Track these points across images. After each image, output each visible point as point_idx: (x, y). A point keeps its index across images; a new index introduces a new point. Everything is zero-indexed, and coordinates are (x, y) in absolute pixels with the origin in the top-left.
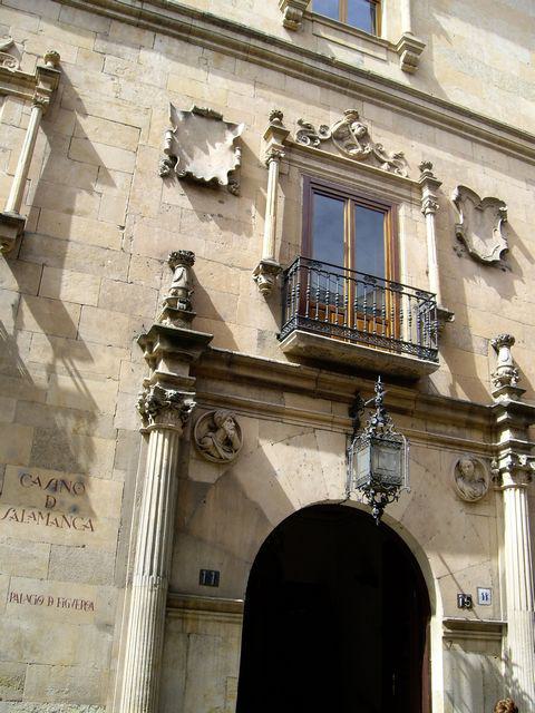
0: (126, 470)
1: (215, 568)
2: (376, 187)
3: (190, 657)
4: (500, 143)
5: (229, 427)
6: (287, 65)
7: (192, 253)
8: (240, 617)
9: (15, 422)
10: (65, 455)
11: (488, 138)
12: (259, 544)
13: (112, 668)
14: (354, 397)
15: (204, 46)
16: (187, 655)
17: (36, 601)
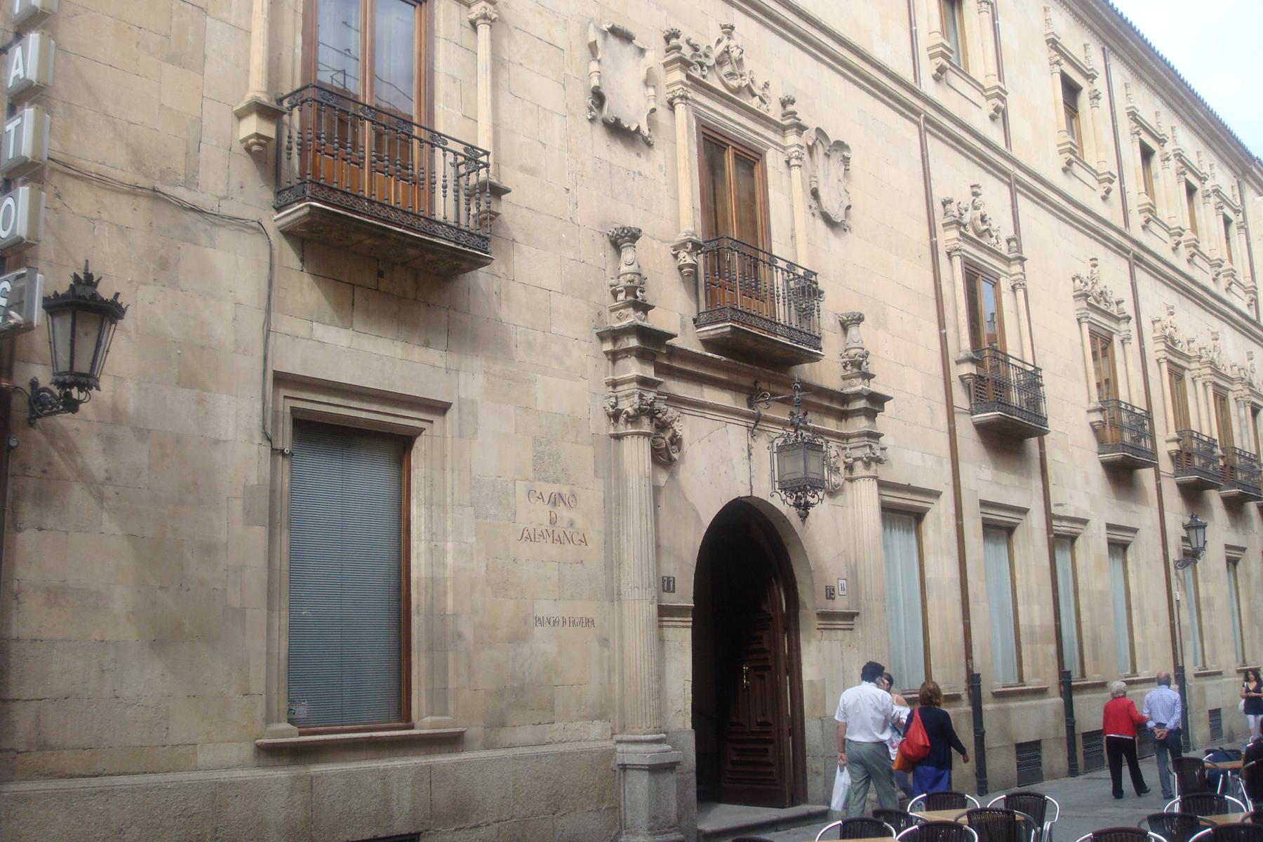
1: (672, 574)
7: (640, 231)
9: (516, 432)
12: (699, 544)
17: (554, 622)
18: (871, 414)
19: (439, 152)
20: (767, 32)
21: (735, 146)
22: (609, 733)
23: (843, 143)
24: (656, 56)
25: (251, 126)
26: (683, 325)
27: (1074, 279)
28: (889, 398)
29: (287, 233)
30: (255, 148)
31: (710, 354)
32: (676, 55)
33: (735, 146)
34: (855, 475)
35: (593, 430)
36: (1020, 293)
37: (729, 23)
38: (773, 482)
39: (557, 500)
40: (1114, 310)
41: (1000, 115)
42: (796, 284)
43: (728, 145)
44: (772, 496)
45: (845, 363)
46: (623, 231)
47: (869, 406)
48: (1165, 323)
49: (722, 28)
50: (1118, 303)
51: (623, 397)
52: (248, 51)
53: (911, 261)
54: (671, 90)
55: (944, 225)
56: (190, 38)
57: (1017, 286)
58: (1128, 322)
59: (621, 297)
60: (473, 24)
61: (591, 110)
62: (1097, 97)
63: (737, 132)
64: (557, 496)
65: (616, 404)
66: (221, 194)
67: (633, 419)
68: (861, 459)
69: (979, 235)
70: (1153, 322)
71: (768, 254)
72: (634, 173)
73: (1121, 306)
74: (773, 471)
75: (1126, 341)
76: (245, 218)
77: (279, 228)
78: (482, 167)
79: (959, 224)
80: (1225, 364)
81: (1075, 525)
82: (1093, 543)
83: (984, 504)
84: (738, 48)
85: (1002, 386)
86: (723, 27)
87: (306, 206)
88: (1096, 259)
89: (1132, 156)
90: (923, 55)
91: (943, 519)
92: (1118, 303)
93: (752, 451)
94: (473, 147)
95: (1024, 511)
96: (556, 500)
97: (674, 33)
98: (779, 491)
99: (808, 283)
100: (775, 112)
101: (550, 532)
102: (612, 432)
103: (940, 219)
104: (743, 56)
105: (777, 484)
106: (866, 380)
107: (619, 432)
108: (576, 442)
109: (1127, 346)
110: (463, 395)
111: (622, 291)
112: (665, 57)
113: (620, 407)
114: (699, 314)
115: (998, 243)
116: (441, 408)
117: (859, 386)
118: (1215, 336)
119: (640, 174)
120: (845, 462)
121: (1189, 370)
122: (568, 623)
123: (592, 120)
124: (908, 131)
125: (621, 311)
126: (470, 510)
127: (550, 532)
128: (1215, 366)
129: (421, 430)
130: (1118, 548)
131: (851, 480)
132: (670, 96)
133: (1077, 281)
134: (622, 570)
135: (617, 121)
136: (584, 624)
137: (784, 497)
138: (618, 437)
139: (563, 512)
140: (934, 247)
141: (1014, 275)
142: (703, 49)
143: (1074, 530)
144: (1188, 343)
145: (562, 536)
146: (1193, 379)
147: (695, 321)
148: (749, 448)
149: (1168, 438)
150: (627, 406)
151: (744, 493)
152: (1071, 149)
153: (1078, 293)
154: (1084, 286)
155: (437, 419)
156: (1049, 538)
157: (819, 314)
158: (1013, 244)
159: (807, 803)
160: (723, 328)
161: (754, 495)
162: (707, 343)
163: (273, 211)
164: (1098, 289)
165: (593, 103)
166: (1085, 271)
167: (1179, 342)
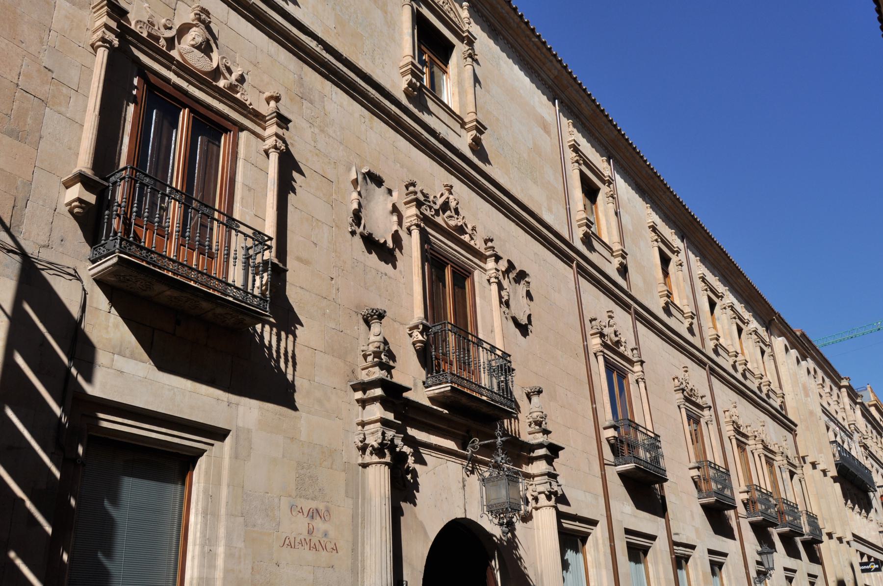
0: (353, 498)
7: (385, 312)
9: (284, 456)
14: (465, 434)
18: (549, 460)
19: (233, 232)
20: (474, 194)
21: (453, 265)
23: (525, 272)
24: (398, 196)
25: (76, 191)
26: (415, 385)
27: (674, 379)
28: (562, 448)
29: (99, 281)
30: (76, 210)
31: (435, 407)
32: (413, 197)
33: (453, 265)
34: (539, 505)
35: (345, 460)
36: (642, 385)
37: (450, 184)
38: (483, 505)
39: (315, 514)
40: (699, 401)
41: (623, 270)
42: (496, 363)
43: (448, 264)
44: (481, 517)
45: (530, 422)
46: (372, 312)
47: (549, 453)
48: (731, 413)
49: (445, 187)
50: (702, 397)
51: (370, 434)
52: (80, 139)
53: (571, 356)
54: (409, 220)
55: (592, 335)
56: (29, 121)
57: (640, 380)
58: (710, 410)
59: (370, 358)
60: (267, 152)
61: (352, 225)
62: (681, 265)
63: (455, 256)
64: (315, 511)
65: (365, 439)
66: (42, 243)
67: (379, 451)
68: (543, 493)
69: (612, 347)
70: (724, 412)
71: (475, 337)
72: (382, 273)
73: (704, 399)
74: (482, 497)
75: (709, 422)
76: (63, 264)
77: (92, 276)
78: (266, 249)
79: (602, 335)
80: (770, 442)
81: (687, 550)
82: (699, 562)
83: (628, 532)
84: (455, 200)
85: (633, 446)
86: (446, 186)
87: (115, 256)
88: (687, 367)
89: (705, 306)
90: (575, 225)
91: (600, 542)
92: (702, 397)
93: (465, 483)
94: (260, 233)
95: (653, 538)
96: (313, 514)
97: (412, 183)
98: (487, 513)
99: (505, 362)
100: (479, 245)
101: (308, 540)
102: (360, 461)
103: (589, 331)
104: (458, 206)
105: (485, 507)
106: (545, 435)
107: (365, 462)
108: (331, 468)
109: (710, 426)
110: (241, 424)
111: (370, 355)
112: (406, 198)
113: (367, 442)
114: (427, 378)
115: (626, 350)
116: (219, 434)
117: (540, 438)
118: (763, 424)
119: (386, 275)
120: (532, 495)
121: (749, 445)
123: (353, 233)
124: (568, 273)
125: (370, 369)
126: (241, 519)
127: (308, 540)
128: (765, 443)
129: (204, 451)
130: (716, 567)
131: (537, 509)
132: (409, 224)
133: (676, 380)
134: (365, 574)
135: (370, 235)
137: (491, 518)
138: (365, 466)
139: (318, 524)
140: (586, 349)
141: (637, 372)
142: (431, 198)
143: (687, 553)
144: (747, 427)
145: (317, 544)
146: (752, 451)
147: (424, 383)
148: (464, 480)
149: (741, 490)
150: (373, 441)
151: (460, 515)
152: (667, 294)
153: (678, 388)
154: (681, 384)
155: (217, 443)
156: (671, 558)
157: (512, 384)
158: (635, 352)
160: (446, 388)
161: (467, 517)
162: (431, 399)
163: (89, 263)
164: (690, 387)
165: (353, 220)
166: (681, 374)
167: (741, 426)
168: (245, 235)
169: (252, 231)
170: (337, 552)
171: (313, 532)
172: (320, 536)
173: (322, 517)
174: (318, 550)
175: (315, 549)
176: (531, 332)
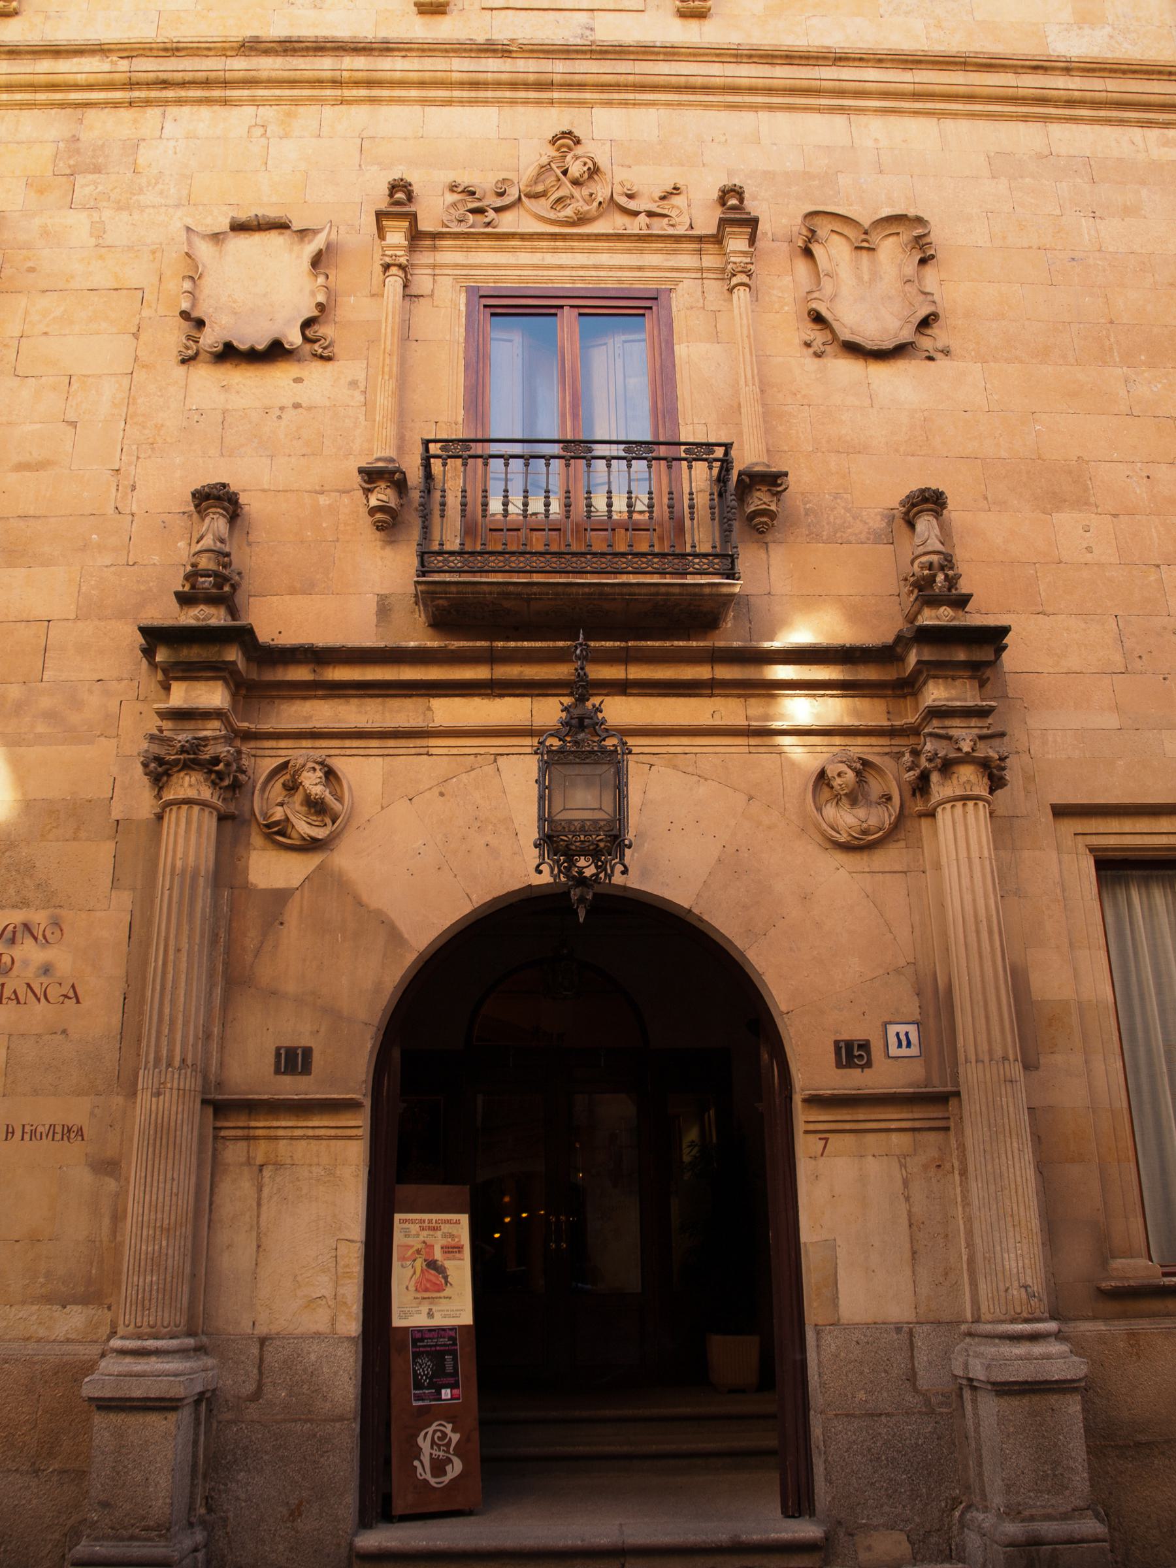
1: (305, 1042)
2: (621, 268)
3: (264, 1209)
4: (916, 96)
5: (312, 783)
6: (422, 84)
8: (360, 1122)
10: (27, 881)
11: (885, 95)
13: (119, 1238)
15: (254, 102)
16: (259, 1205)
22: (105, 1330)
64: (20, 929)
122: (18, 1133)
136: (58, 1137)
159: (391, 1493)
168: (548, 458)
169: (622, 446)
170: (78, 1002)
171: (11, 969)
172: (31, 975)
173: (40, 937)
174: (22, 1001)
175: (15, 1002)
176: (630, 196)
